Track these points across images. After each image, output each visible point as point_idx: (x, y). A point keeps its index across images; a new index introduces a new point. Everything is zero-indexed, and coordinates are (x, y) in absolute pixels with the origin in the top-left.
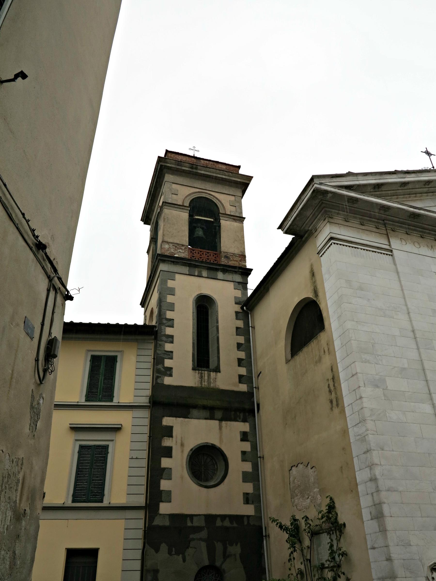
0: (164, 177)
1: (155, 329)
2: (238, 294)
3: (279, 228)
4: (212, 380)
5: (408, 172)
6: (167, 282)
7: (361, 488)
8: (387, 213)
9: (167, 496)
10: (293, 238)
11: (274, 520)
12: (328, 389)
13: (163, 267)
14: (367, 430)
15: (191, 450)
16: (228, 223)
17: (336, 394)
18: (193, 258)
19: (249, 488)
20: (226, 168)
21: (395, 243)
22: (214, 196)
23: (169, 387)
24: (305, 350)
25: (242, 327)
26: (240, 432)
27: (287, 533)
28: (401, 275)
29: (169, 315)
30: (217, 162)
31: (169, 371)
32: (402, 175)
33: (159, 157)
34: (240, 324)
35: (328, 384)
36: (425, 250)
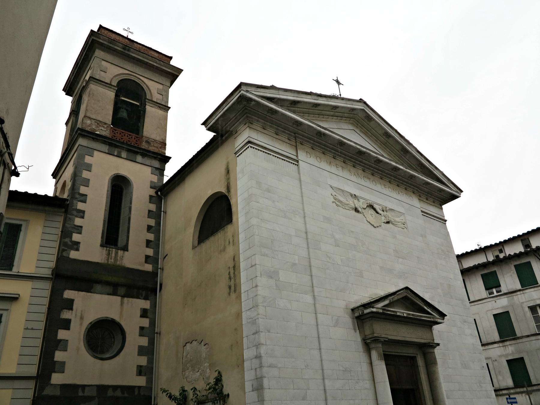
0: (94, 52)
1: (66, 202)
2: (155, 179)
3: (203, 124)
4: (119, 258)
5: (320, 96)
6: (84, 157)
7: (246, 364)
8: (299, 128)
9: (61, 367)
10: (214, 136)
11: (164, 391)
12: (228, 276)
13: (82, 141)
14: (258, 314)
15: (91, 323)
16: (153, 109)
17: (235, 281)
18: (114, 138)
19: (143, 361)
20: (158, 57)
21: (302, 156)
22: (143, 81)
23: (75, 260)
24: (212, 239)
25: (155, 210)
26: (141, 309)
27: (175, 402)
28: (302, 183)
29: (83, 190)
30: (151, 49)
31: (76, 246)
32: (315, 97)
33: (92, 31)
34: (153, 207)
35: (228, 272)
36: (324, 165)
